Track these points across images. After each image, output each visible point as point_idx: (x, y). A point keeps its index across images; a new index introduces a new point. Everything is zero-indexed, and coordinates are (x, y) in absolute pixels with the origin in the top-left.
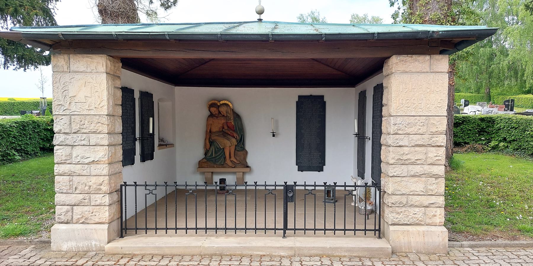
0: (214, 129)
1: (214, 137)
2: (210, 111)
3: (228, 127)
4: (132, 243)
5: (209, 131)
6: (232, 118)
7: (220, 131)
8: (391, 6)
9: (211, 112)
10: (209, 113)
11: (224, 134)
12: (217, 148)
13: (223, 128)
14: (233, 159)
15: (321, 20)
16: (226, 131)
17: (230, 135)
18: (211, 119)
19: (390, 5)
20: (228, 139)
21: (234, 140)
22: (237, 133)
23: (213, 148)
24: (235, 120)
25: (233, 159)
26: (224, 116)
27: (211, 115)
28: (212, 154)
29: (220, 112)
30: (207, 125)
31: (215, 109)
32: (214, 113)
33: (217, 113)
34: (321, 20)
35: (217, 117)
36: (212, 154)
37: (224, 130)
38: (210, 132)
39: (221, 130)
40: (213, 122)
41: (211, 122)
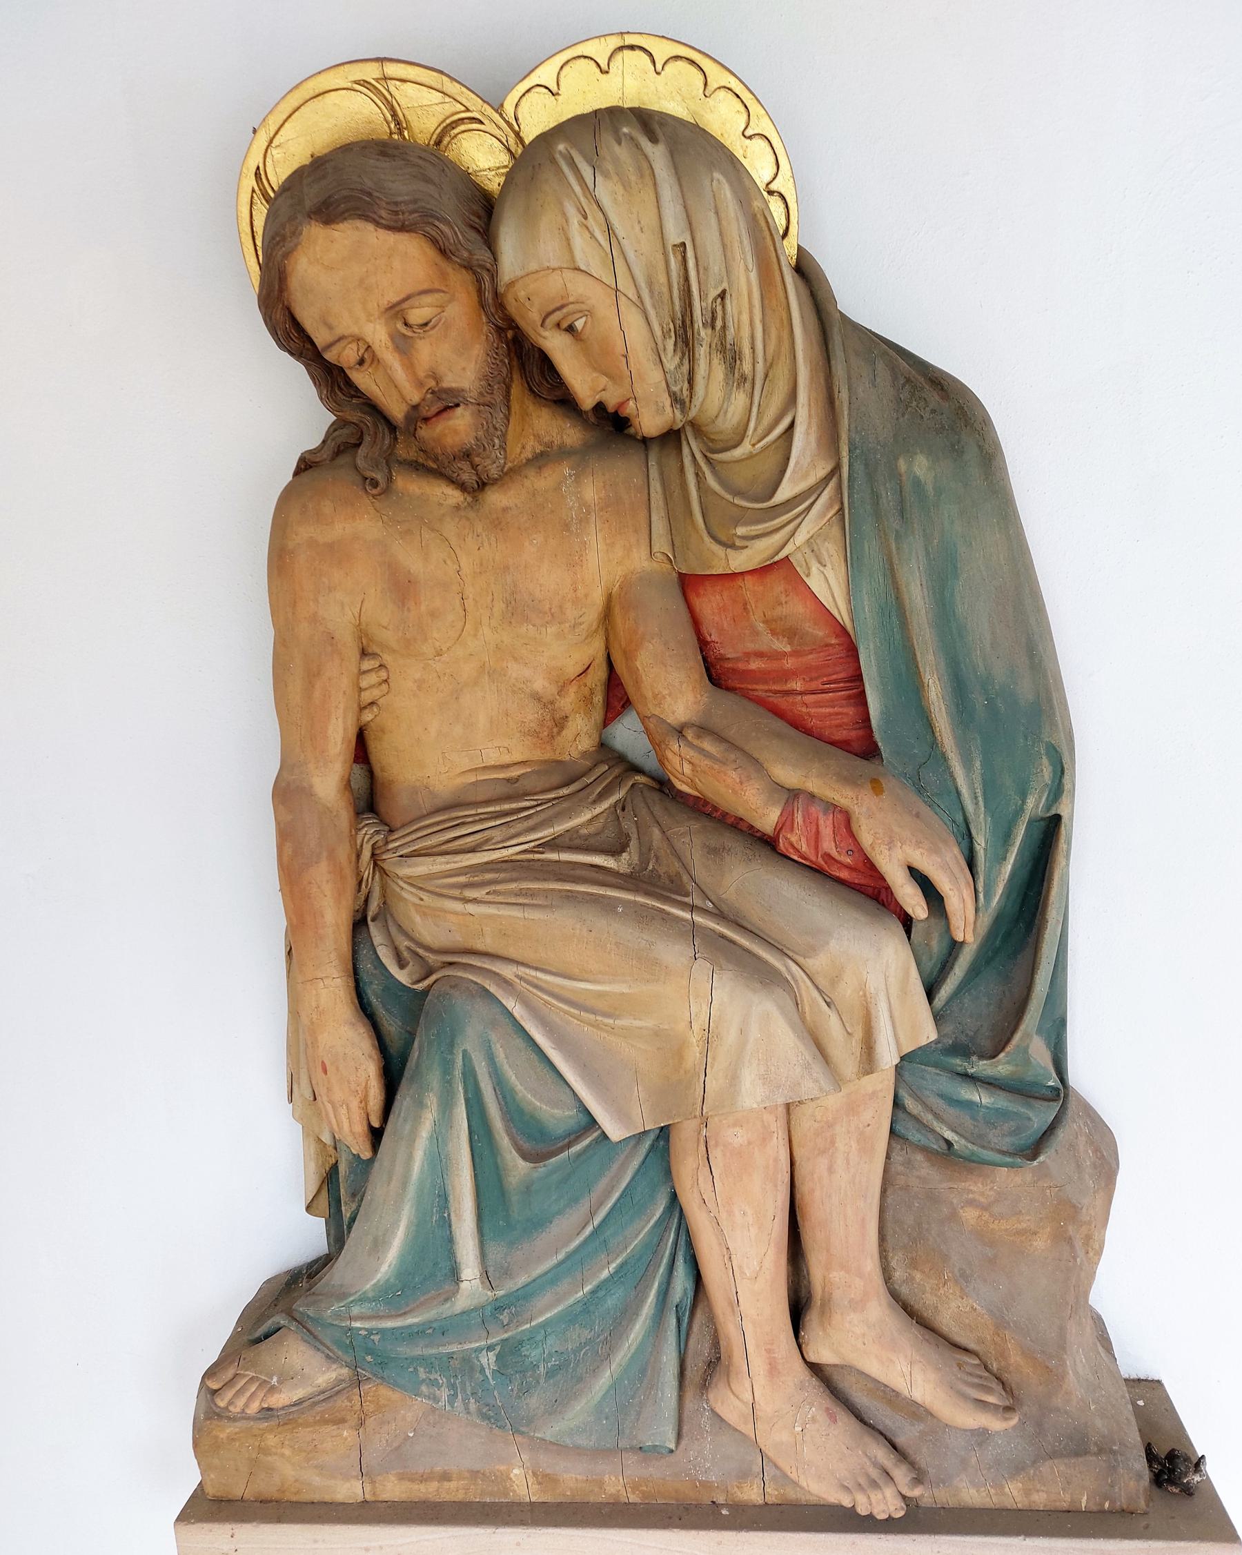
0: (455, 737)
1: (439, 908)
2: (292, 334)
3: (716, 673)
4: (789, 277)
5: (329, 781)
6: (806, 463)
7: (568, 780)
8: (1191, 1494)
9: (332, 379)
10: (296, 416)
11: (627, 818)
12: (539, 1144)
13: (616, 696)
14: (861, 1335)
15: (861, 732)
16: (686, 767)
17: (768, 844)
18: (355, 523)
19: (1204, 1464)
20: (744, 948)
21: (876, 971)
22: (927, 781)
23: (432, 1134)
24: (870, 500)
25: (861, 1335)
26: (612, 425)
27: (366, 442)
28: (432, 1263)
29: (524, 363)
30: (296, 666)
31: (399, 262)
32: (393, 386)
33: (461, 360)
34: (861, 732)
35: (473, 477)
36: (432, 1263)
37: (627, 735)
38: (370, 798)
39: (579, 737)
40: (402, 588)
41: (350, 600)
